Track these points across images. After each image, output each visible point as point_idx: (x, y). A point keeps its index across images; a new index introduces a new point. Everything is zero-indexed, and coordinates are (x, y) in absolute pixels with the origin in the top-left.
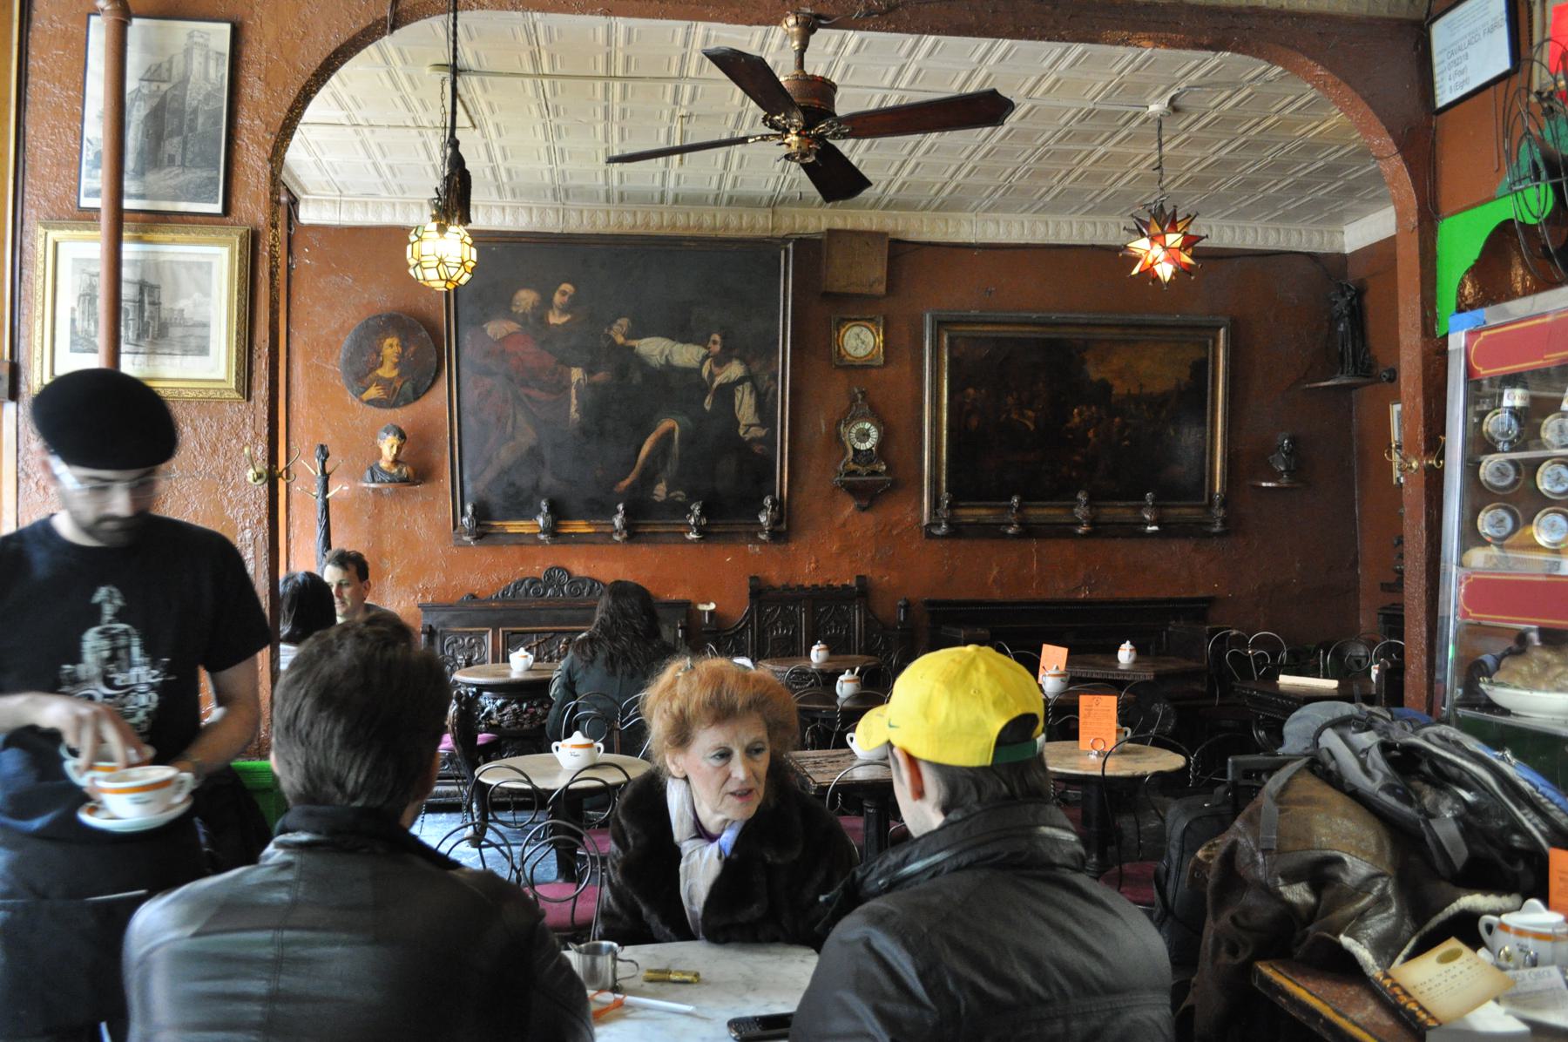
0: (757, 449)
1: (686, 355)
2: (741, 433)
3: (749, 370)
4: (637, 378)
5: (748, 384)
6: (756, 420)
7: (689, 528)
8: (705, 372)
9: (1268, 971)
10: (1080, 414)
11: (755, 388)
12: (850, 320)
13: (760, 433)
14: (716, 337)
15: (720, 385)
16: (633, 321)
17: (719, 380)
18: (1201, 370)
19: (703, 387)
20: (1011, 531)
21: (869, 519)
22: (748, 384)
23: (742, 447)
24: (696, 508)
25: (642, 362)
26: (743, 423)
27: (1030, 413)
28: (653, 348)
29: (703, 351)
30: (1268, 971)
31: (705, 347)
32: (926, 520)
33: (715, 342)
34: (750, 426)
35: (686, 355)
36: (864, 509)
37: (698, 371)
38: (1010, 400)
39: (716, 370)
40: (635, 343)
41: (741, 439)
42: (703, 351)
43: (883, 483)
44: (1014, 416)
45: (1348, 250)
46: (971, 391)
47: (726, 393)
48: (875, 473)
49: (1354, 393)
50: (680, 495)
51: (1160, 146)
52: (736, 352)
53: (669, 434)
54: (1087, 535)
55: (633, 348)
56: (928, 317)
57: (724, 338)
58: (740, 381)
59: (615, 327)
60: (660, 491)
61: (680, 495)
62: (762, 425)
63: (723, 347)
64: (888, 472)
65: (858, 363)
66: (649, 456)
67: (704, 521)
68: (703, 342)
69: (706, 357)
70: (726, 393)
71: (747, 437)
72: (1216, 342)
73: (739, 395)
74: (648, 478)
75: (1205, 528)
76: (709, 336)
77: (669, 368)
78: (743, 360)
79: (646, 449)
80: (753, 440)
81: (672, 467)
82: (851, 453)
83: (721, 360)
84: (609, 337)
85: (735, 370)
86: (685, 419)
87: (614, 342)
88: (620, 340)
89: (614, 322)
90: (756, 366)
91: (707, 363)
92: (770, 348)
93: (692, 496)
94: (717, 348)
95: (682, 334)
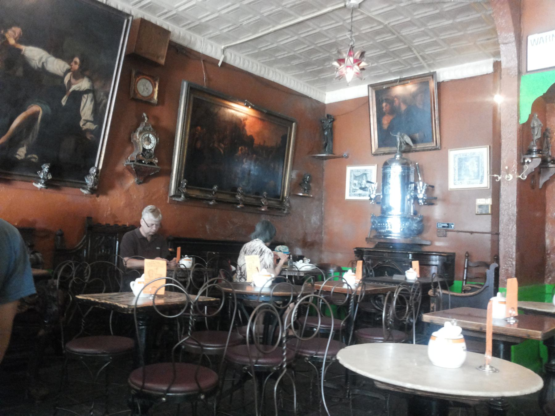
0: (89, 136)
1: (56, 66)
2: (81, 124)
3: (93, 86)
4: (20, 72)
5: (91, 95)
6: (91, 118)
7: (37, 180)
8: (66, 80)
9: (80, 297)
10: (242, 149)
11: (94, 98)
12: (144, 74)
13: (90, 126)
14: (77, 60)
15: (74, 91)
16: (24, 31)
17: (74, 87)
18: (285, 140)
19: (63, 90)
20: (211, 203)
21: (142, 188)
22: (91, 95)
23: (80, 134)
24: (46, 168)
25: (25, 62)
26: (83, 118)
27: (222, 145)
28: (35, 54)
29: (67, 66)
30: (80, 297)
31: (70, 64)
32: (172, 192)
33: (76, 63)
34: (87, 121)
35: (56, 66)
36: (140, 183)
37: (62, 78)
38: (215, 137)
39: (73, 81)
40: (23, 47)
41: (80, 128)
42: (67, 66)
43: (155, 169)
44: (216, 145)
45: (326, 102)
46: (199, 128)
47: (77, 96)
48: (151, 163)
49: (325, 161)
50: (34, 158)
51: (352, 18)
52: (87, 73)
53: (34, 116)
54: (213, 207)
55: (20, 50)
56: (185, 84)
57: (82, 61)
58: (87, 92)
59: (10, 32)
60: (21, 153)
61: (34, 158)
62: (94, 122)
63: (80, 67)
64: (158, 164)
65: (144, 100)
66: (19, 127)
67: (50, 177)
68: (69, 60)
69: (68, 71)
70: (77, 96)
71: (85, 128)
72: (291, 128)
73: (84, 100)
74: (14, 142)
75: (259, 208)
76: (73, 57)
77: (43, 71)
78: (90, 79)
79: (17, 121)
80: (87, 130)
81: (32, 138)
82: (142, 149)
83: (78, 75)
84: (4, 37)
85: (84, 84)
86: (48, 108)
87: (7, 41)
88: (12, 41)
89: (10, 27)
90: (98, 85)
91: (69, 75)
92: (108, 77)
93: (43, 160)
94: (76, 67)
95: (57, 51)
